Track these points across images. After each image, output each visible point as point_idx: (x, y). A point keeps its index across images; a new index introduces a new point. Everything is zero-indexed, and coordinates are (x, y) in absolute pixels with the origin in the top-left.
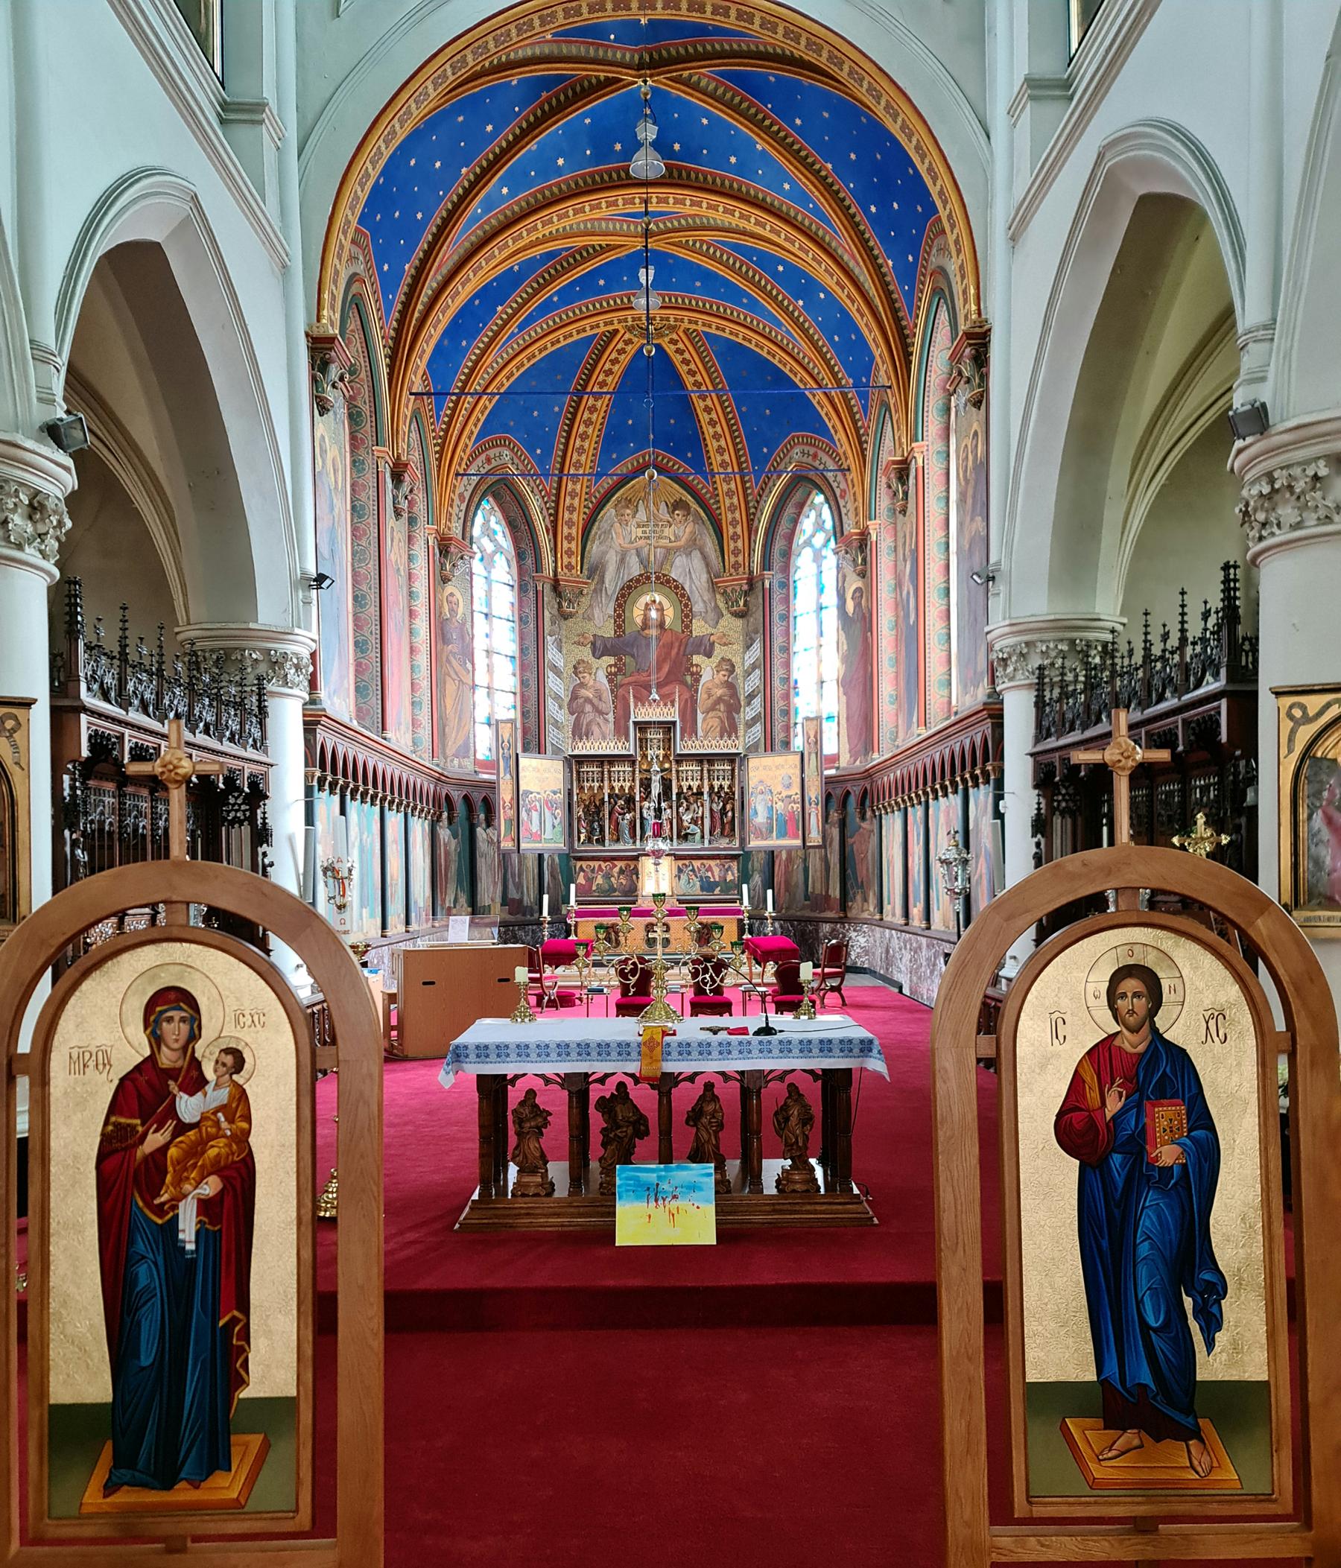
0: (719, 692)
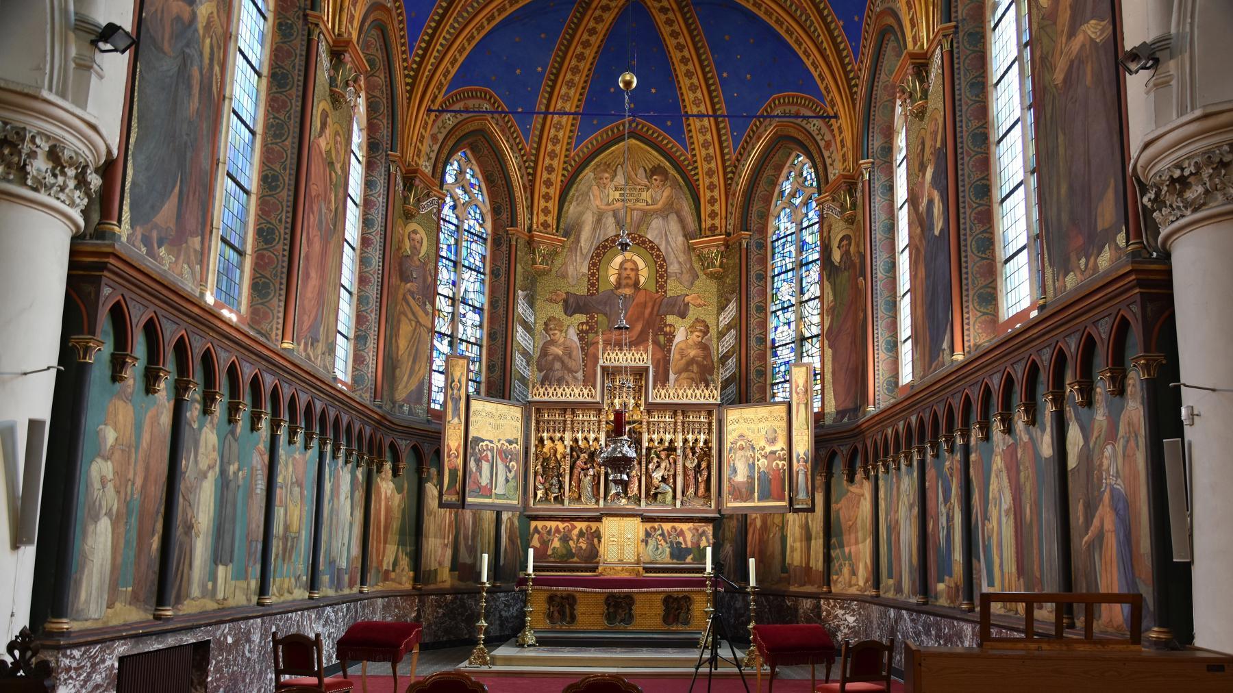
0: (692, 353)
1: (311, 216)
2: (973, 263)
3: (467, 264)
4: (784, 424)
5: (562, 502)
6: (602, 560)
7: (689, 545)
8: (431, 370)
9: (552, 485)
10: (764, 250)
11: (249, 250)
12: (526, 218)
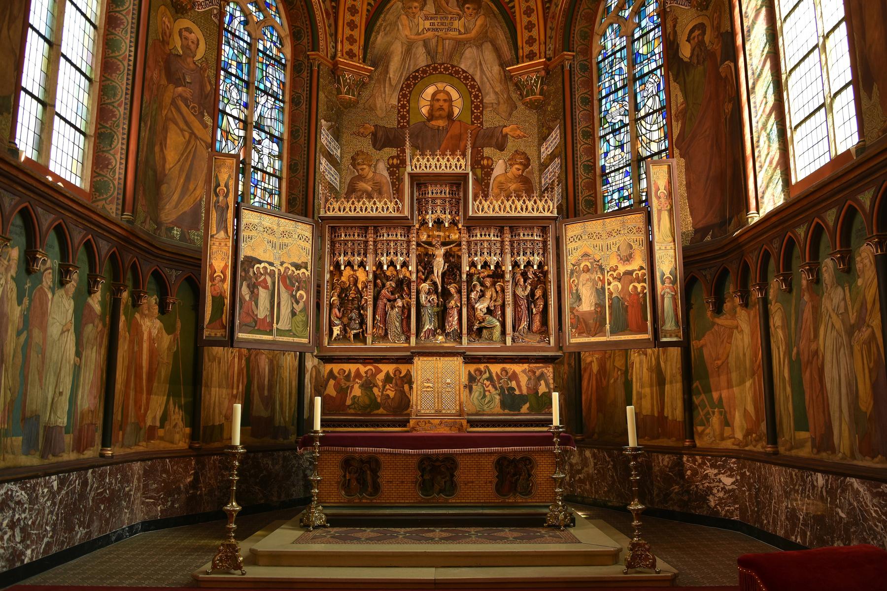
3: (262, 87)
6: (414, 410)
7: (525, 391)
9: (351, 319)
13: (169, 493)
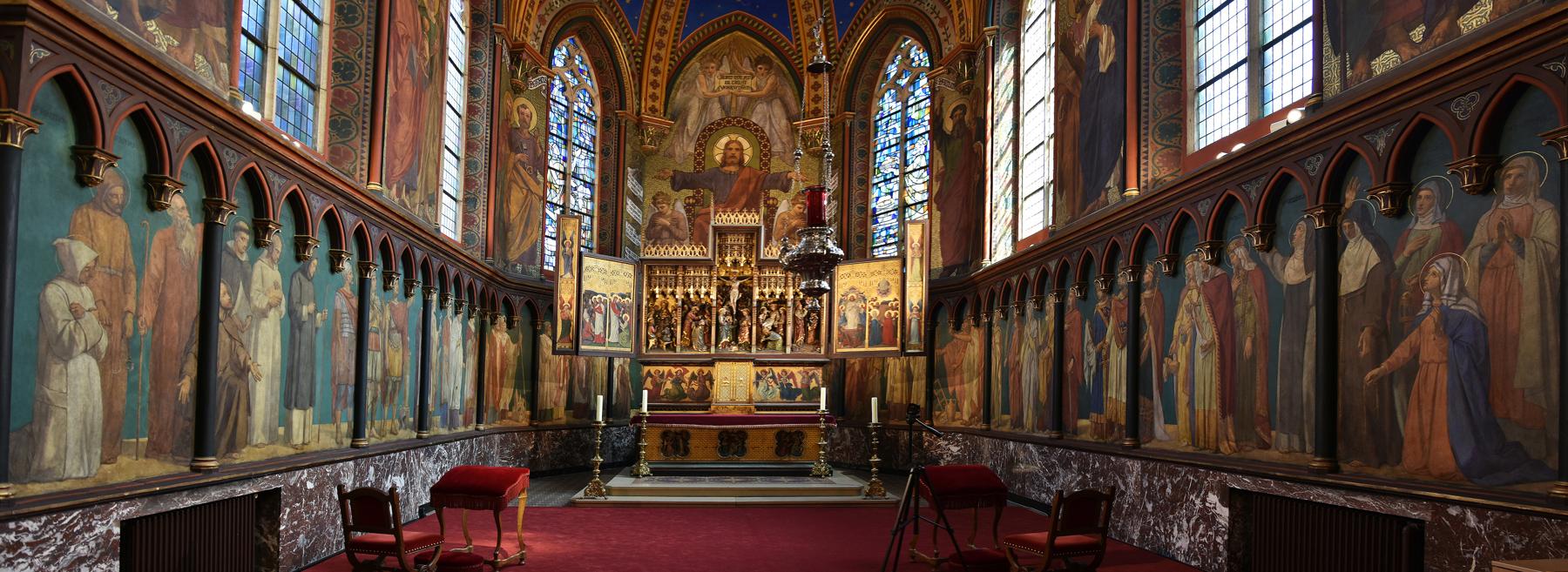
0: (794, 223)
1: (399, 56)
2: (1155, 93)
3: (577, 142)
4: (898, 277)
5: (674, 349)
7: (799, 386)
8: (543, 236)
9: (664, 334)
10: (867, 129)
11: (323, 84)
12: (635, 103)
13: (517, 456)
